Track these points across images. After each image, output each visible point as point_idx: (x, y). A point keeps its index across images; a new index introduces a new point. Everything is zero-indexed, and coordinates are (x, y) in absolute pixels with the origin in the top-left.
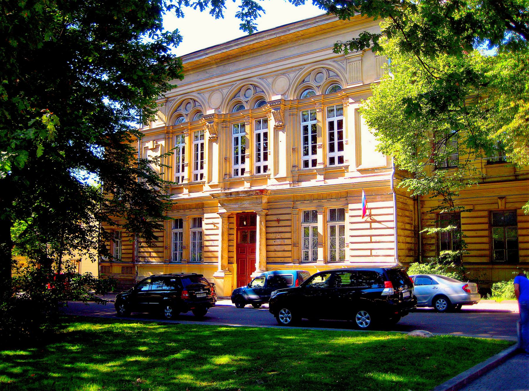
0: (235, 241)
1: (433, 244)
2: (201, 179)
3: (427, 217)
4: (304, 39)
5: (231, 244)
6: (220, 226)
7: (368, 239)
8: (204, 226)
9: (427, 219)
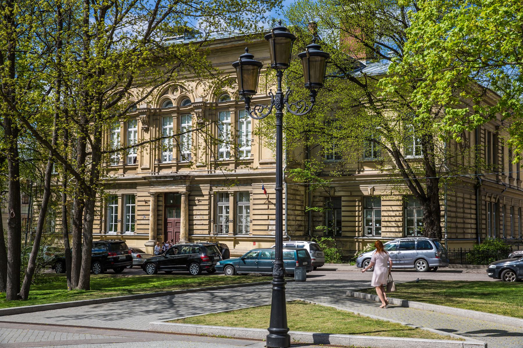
0: (163, 216)
1: (320, 221)
2: (135, 162)
3: (317, 200)
4: (222, 52)
5: (160, 218)
6: (151, 203)
7: (266, 217)
8: (137, 203)
9: (317, 201)
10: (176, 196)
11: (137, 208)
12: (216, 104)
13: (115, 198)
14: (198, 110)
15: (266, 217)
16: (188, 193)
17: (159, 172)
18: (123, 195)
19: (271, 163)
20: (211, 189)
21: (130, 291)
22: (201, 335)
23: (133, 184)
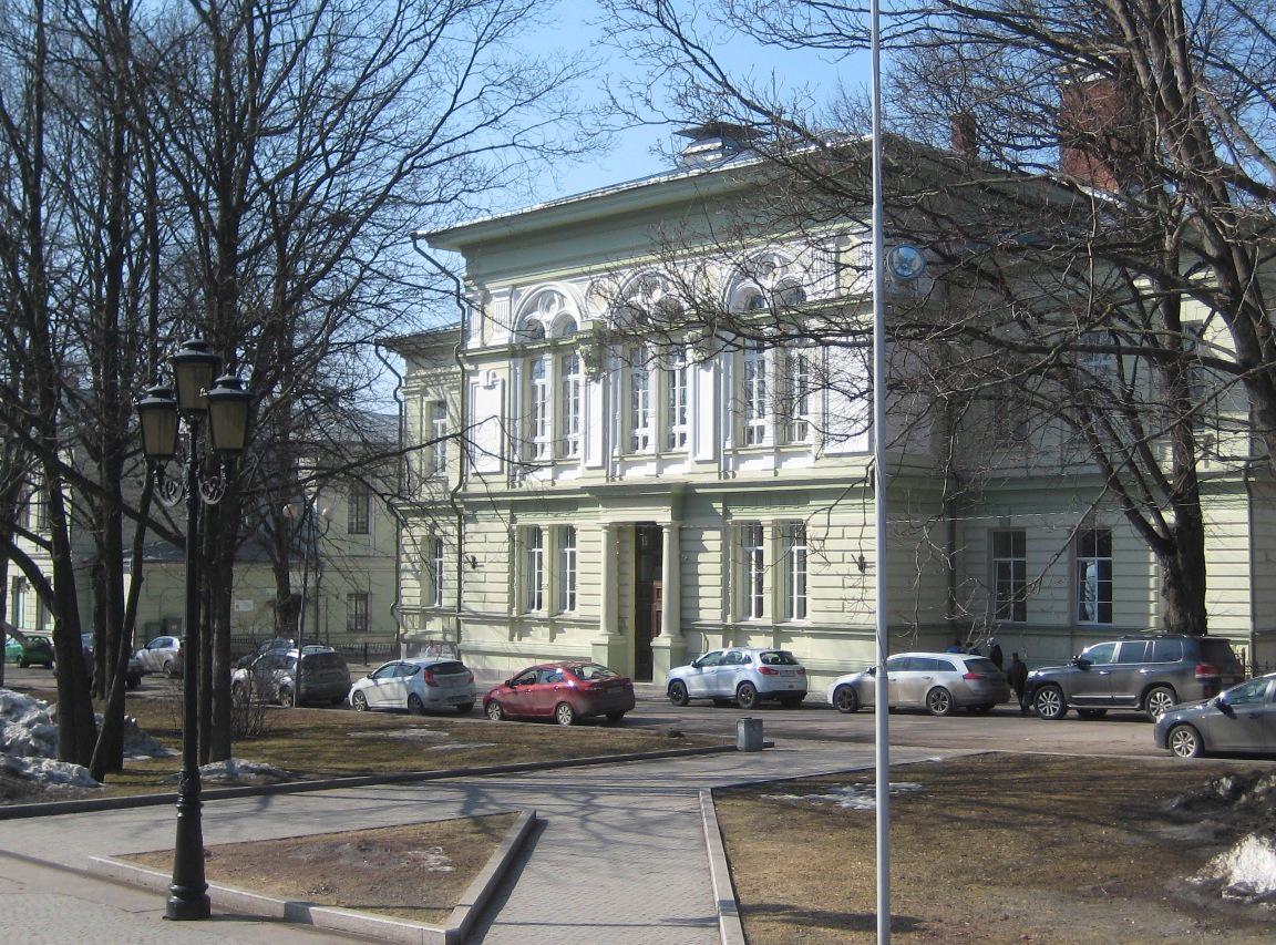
7: (837, 581)
12: (523, 346)
13: (536, 533)
16: (677, 525)
17: (736, 467)
18: (552, 528)
20: (513, 520)
21: (632, 811)
22: (416, 908)
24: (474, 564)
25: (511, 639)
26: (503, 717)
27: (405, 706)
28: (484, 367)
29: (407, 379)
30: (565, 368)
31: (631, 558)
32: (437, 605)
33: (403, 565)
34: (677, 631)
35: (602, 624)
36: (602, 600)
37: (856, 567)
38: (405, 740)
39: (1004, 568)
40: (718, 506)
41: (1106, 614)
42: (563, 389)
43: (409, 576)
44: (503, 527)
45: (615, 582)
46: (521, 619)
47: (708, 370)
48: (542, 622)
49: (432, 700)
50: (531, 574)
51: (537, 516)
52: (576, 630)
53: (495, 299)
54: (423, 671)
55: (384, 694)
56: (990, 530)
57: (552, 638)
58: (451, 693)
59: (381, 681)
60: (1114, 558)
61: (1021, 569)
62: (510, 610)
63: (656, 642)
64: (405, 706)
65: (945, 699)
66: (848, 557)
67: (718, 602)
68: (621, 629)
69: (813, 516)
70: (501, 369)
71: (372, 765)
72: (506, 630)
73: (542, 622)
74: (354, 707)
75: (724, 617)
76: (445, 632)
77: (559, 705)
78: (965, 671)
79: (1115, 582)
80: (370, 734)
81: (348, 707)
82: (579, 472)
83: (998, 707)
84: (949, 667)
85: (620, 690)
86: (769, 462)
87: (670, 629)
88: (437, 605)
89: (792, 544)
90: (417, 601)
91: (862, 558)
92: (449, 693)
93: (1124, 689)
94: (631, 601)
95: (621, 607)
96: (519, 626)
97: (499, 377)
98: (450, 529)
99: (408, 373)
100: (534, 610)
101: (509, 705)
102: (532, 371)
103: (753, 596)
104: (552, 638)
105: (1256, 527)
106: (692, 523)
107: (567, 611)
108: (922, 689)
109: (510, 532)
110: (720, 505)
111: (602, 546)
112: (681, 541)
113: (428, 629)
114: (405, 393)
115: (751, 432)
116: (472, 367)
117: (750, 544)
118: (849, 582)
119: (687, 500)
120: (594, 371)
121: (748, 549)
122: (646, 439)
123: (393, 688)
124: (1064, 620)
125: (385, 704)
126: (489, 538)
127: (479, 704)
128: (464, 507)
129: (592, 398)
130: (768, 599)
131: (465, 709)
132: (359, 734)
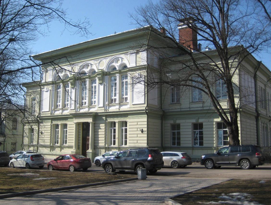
10: (87, 124)
11: (68, 131)
13: (57, 126)
14: (99, 76)
15: (136, 136)
16: (94, 122)
17: (109, 108)
18: (61, 124)
19: (190, 131)
23: (65, 118)
24: (42, 133)
25: (50, 151)
26: (53, 169)
27: (25, 166)
28: (46, 87)
29: (26, 93)
30: (65, 87)
31: (81, 131)
32: (32, 144)
33: (24, 135)
34: (93, 148)
35: (74, 147)
36: (74, 141)
37: (141, 132)
38: (25, 177)
39: (174, 134)
40: (104, 118)
41: (201, 144)
42: (65, 91)
43: (25, 137)
44: (50, 124)
45: (93, 131)
46: (53, 146)
47: (102, 85)
48: (58, 147)
49: (32, 165)
50: (56, 136)
51: (58, 121)
52: (67, 149)
53: (49, 71)
54: (30, 156)
55: (19, 163)
56: (171, 124)
57: (61, 151)
58: (38, 163)
59: (18, 160)
60: (204, 130)
61: (179, 133)
62: (50, 144)
63: (87, 151)
64: (25, 166)
65: (176, 164)
66: (139, 129)
67: (104, 141)
68: (78, 148)
69: (130, 120)
70: (50, 87)
71: (13, 187)
72: (49, 149)
73: (58, 147)
74: (11, 167)
75: (105, 145)
76: (34, 150)
77: (70, 166)
78: (182, 156)
79: (204, 136)
80: (14, 174)
81: (9, 167)
82: (68, 111)
83: (188, 166)
84: (177, 155)
85: (88, 161)
86: (117, 107)
87: (91, 148)
88: (32, 144)
89: (123, 127)
90: (27, 143)
91: (142, 130)
92: (37, 163)
93: (233, 160)
94: (81, 141)
95: (78, 143)
96: (52, 148)
97: (49, 89)
98: (36, 127)
99: (27, 91)
100: (56, 144)
101: (56, 167)
102: (58, 88)
103: (113, 140)
104: (61, 151)
105: (149, 141)
106: (97, 122)
107: (65, 144)
108: (170, 161)
109: (51, 125)
110: (105, 118)
111: (74, 128)
112: (94, 126)
113: (30, 149)
114: (26, 96)
115: (112, 100)
116: (43, 87)
117: (112, 127)
118: (139, 135)
119: (96, 117)
120: (73, 86)
121: (111, 128)
122: (85, 103)
123: (22, 162)
124: (190, 145)
125: (19, 166)
126: (46, 127)
127: (46, 166)
128: (39, 120)
129: (72, 93)
130: (117, 140)
131: (41, 167)
132: (11, 175)
